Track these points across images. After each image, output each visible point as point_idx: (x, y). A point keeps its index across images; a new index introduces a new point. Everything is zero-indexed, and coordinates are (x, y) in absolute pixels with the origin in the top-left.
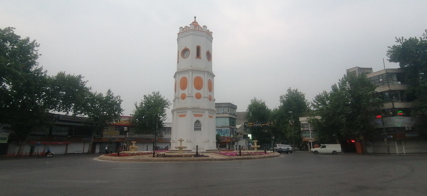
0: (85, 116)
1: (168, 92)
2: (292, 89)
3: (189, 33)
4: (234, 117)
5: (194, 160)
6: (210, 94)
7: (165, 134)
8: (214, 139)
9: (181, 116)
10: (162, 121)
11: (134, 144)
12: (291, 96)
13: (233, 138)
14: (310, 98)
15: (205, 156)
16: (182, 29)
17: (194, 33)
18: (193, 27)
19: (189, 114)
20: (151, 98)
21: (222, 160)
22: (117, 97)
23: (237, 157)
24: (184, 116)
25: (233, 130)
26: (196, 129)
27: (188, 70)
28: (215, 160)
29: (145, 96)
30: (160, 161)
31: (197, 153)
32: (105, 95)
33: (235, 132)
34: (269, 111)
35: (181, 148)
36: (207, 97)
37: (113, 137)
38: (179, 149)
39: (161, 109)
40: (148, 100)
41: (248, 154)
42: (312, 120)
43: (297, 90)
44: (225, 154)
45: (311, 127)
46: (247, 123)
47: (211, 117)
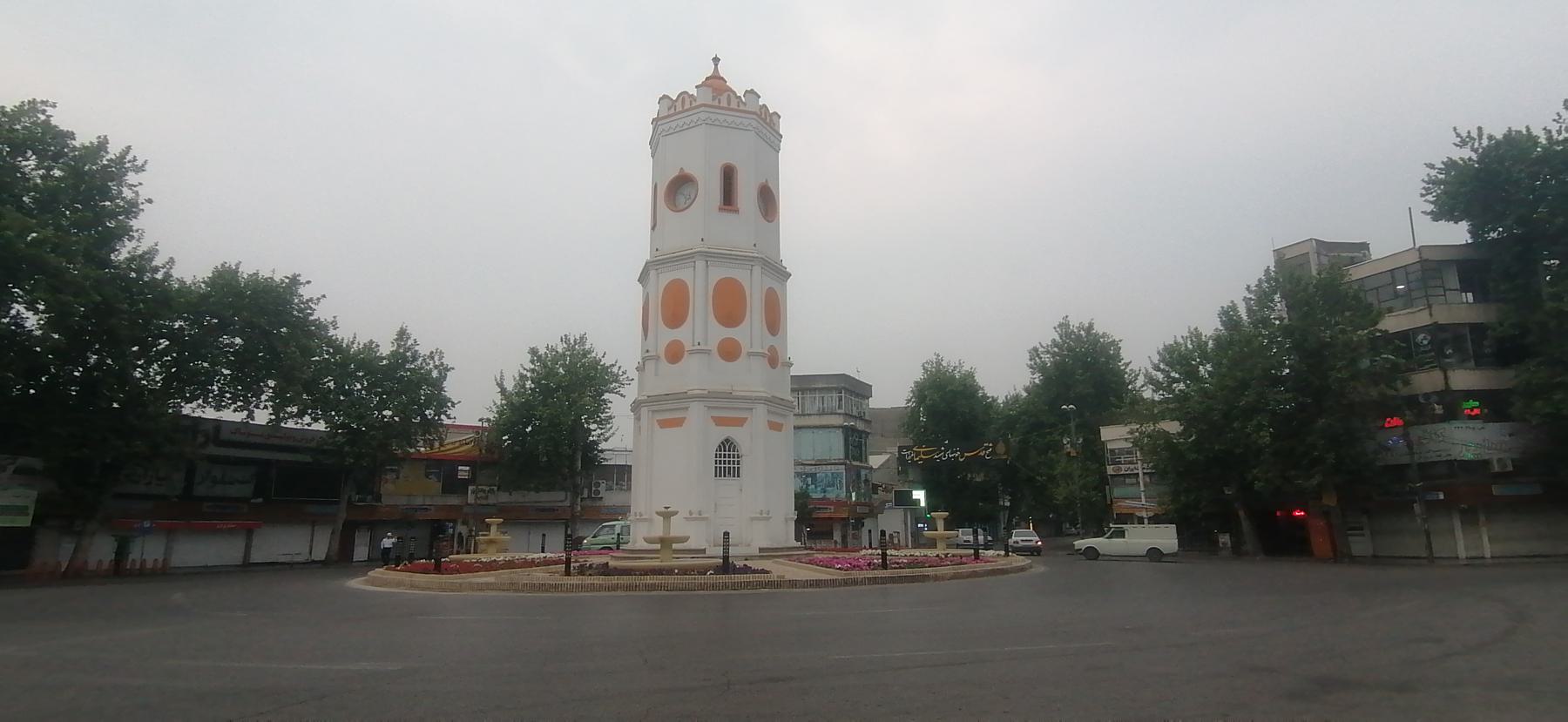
0: (315, 427)
1: (618, 339)
2: (1074, 323)
3: (695, 118)
4: (860, 426)
5: (714, 587)
6: (771, 340)
7: (609, 489)
9: (665, 424)
10: (596, 443)
11: (493, 529)
12: (1070, 349)
13: (857, 504)
14: (1140, 356)
15: (755, 571)
16: (666, 102)
17: (713, 117)
18: (707, 97)
19: (696, 414)
20: (557, 357)
21: (817, 584)
23: (871, 574)
24: (678, 423)
25: (859, 476)
26: (721, 472)
27: (692, 256)
28: (793, 584)
29: (534, 352)
30: (593, 588)
31: (726, 558)
32: (386, 349)
33: (866, 481)
34: (989, 405)
35: (665, 542)
36: (763, 355)
37: (419, 501)
38: (658, 546)
41: (914, 563)
42: (1149, 436)
43: (1091, 326)
44: (827, 565)
45: (1143, 462)
46: (908, 448)
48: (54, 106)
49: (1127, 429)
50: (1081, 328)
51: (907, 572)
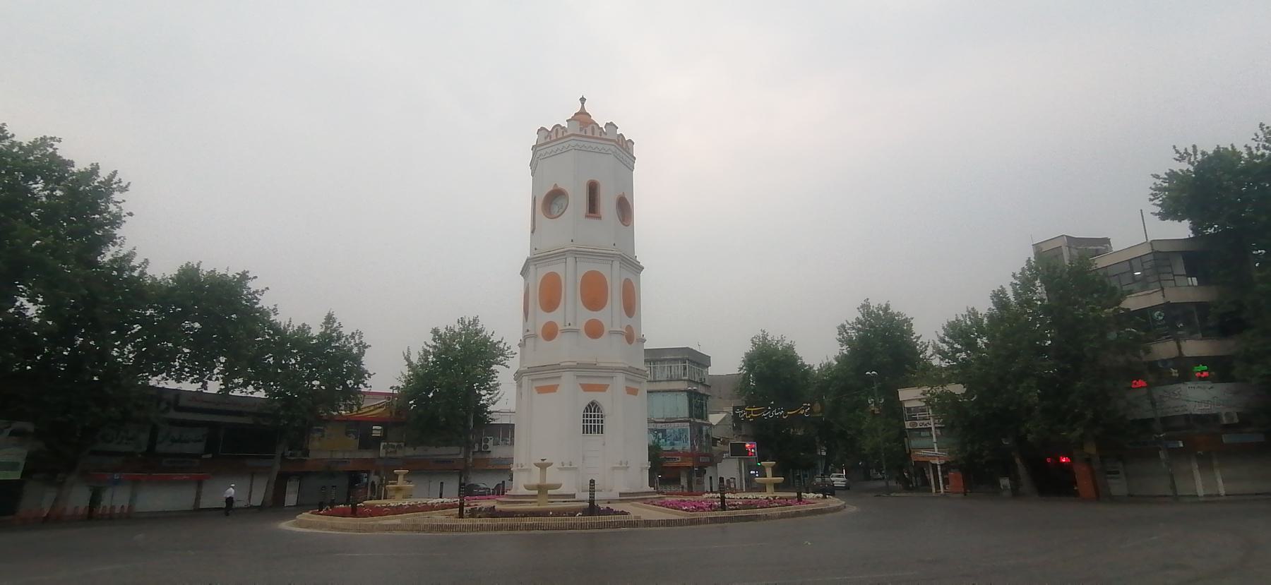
1: (504, 321)
2: (874, 304)
3: (566, 145)
4: (702, 390)
5: (582, 526)
7: (496, 444)
8: (641, 460)
9: (541, 390)
10: (485, 406)
11: (400, 478)
14: (928, 331)
15: (616, 513)
16: (543, 134)
17: (581, 144)
19: (568, 382)
21: (668, 523)
22: (353, 336)
24: (552, 389)
25: (701, 431)
26: (587, 430)
28: (648, 523)
29: (435, 331)
30: (481, 528)
31: (592, 502)
32: (316, 331)
33: (707, 436)
34: (806, 372)
35: (542, 489)
37: (339, 456)
39: (484, 369)
40: (444, 343)
41: (749, 505)
42: (938, 396)
43: (887, 307)
44: (676, 506)
46: (741, 408)
47: (632, 391)
48: (60, 141)
49: (920, 391)
50: (879, 308)
51: (742, 513)
